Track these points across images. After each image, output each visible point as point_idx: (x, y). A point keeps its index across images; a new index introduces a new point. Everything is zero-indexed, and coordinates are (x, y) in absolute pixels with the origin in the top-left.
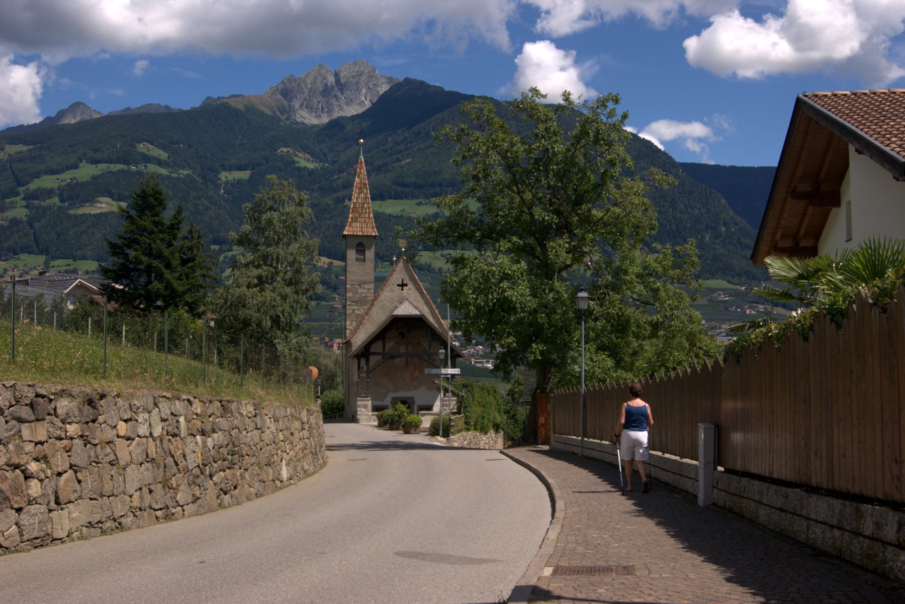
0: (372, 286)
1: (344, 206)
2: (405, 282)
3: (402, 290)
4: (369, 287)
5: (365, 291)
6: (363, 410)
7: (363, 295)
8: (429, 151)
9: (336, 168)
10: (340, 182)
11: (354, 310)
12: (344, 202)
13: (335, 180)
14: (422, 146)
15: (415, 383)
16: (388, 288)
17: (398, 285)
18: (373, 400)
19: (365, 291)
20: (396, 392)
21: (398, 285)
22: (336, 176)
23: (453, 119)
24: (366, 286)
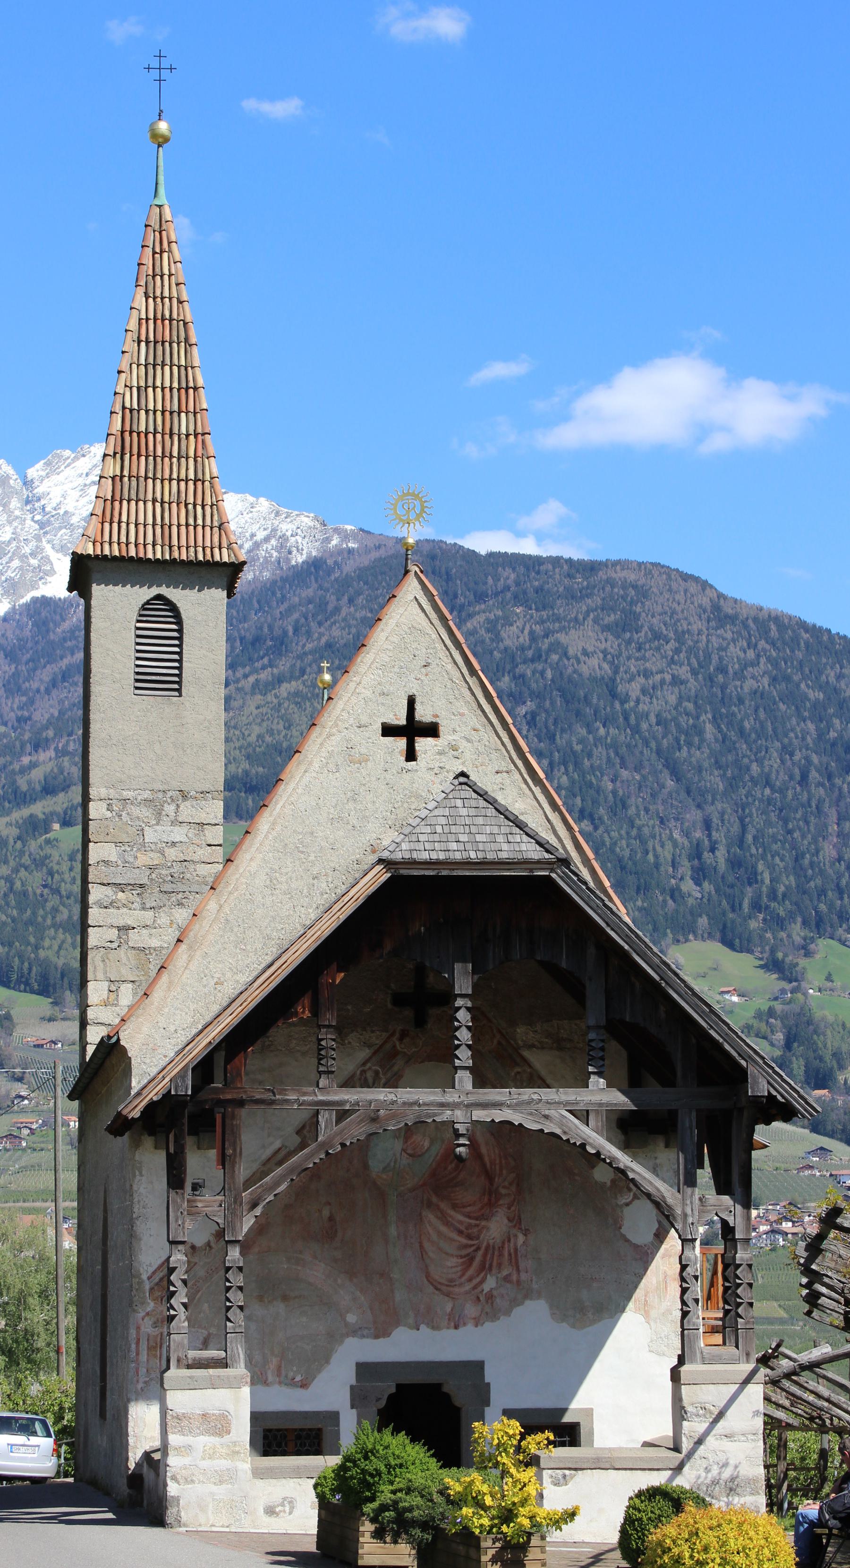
0: (215, 809)
1: (48, 842)
2: (423, 714)
3: (411, 755)
4: (203, 817)
5: (179, 834)
6: (203, 1441)
7: (172, 853)
8: (285, 689)
9: (27, 736)
10: (37, 775)
11: (124, 929)
12: (48, 830)
13: (23, 771)
14: (264, 676)
15: (490, 1283)
16: (335, 743)
17: (389, 731)
18: (258, 1379)
19: (179, 834)
20: (381, 1331)
21: (389, 731)
22: (26, 760)
23: (351, 601)
24: (187, 811)
